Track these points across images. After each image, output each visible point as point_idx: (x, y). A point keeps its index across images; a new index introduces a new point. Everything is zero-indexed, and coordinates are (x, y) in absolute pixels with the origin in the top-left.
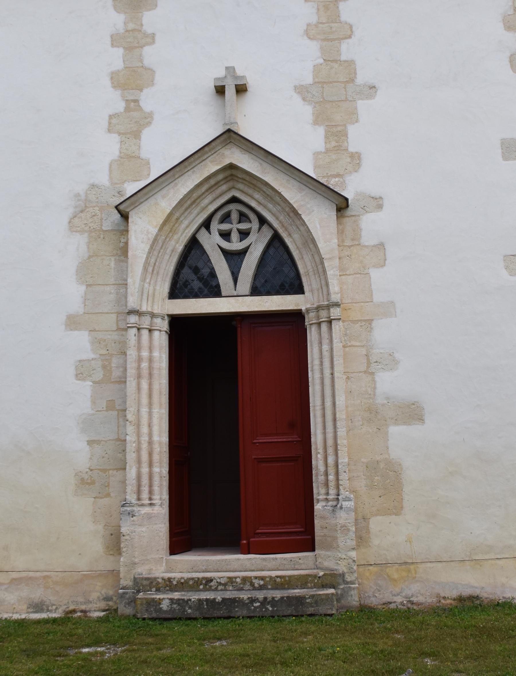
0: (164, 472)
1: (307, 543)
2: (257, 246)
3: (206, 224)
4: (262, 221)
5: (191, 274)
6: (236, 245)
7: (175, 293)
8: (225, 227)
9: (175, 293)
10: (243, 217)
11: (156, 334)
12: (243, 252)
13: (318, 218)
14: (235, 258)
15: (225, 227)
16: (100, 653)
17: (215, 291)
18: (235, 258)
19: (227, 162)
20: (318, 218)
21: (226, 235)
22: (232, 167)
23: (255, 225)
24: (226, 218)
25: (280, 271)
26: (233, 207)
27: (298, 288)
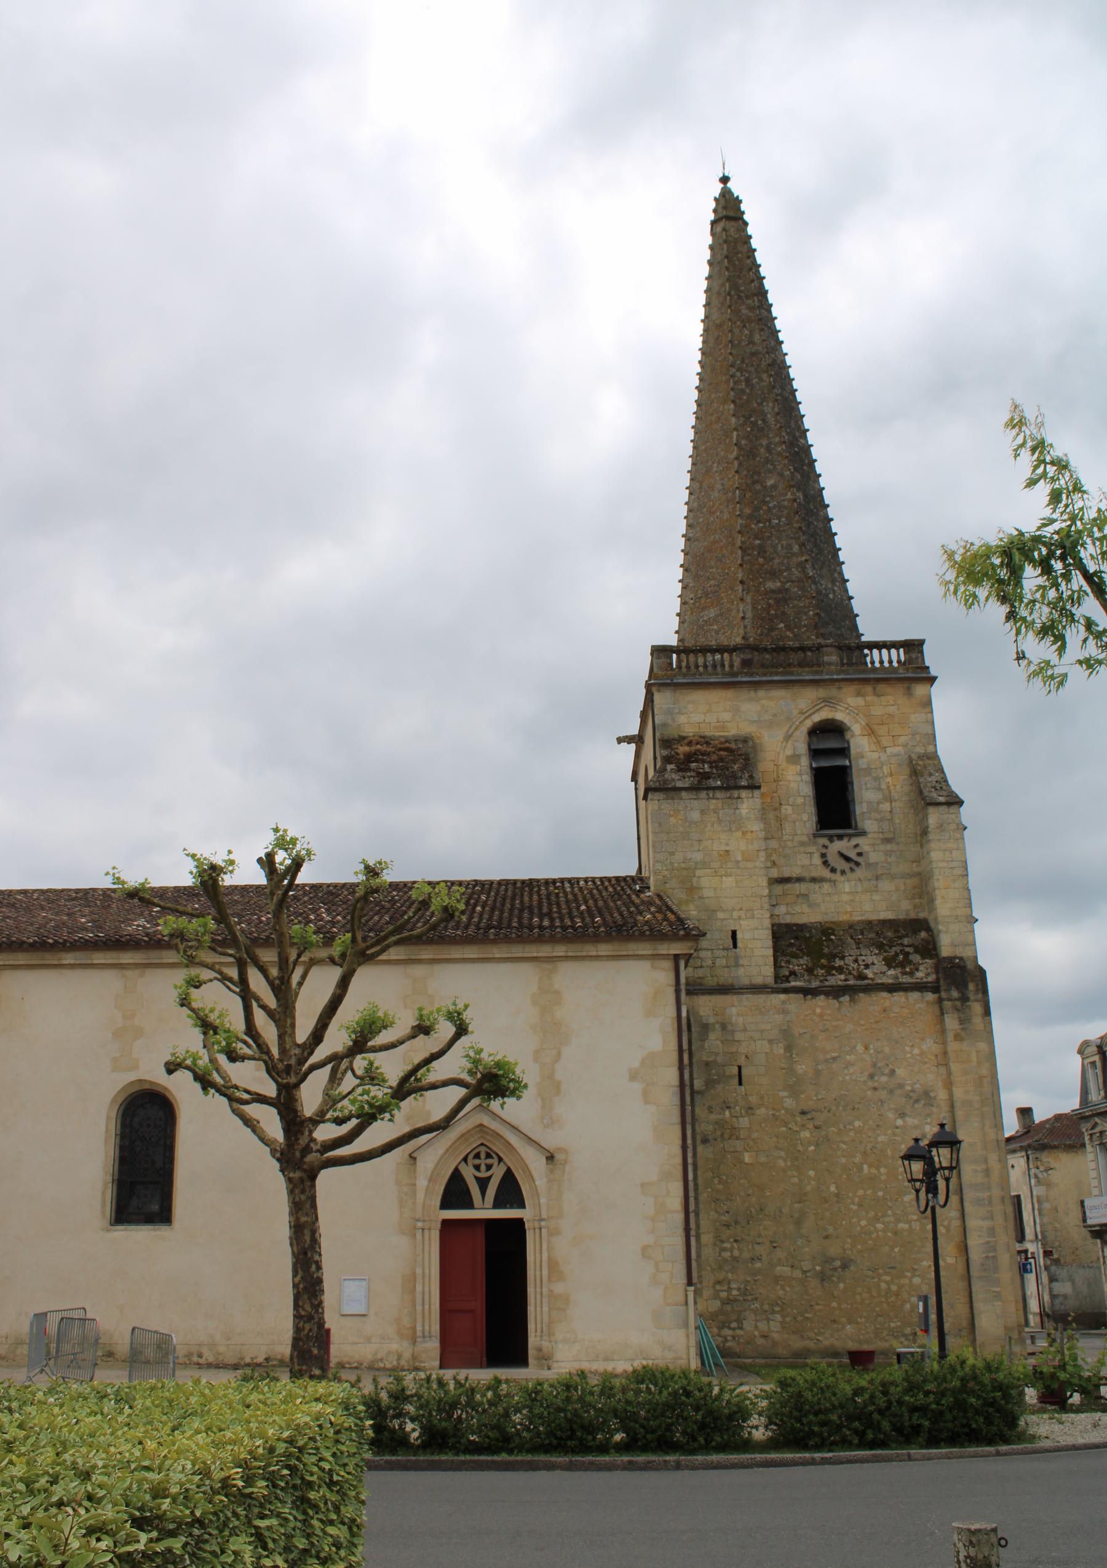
0: (903, 1146)
1: (521, 1359)
2: (498, 1173)
3: (465, 1159)
4: (500, 1160)
5: (455, 1193)
6: (483, 1174)
7: (445, 1204)
8: (477, 1162)
9: (445, 1204)
10: (488, 1156)
11: (433, 1232)
12: (489, 1178)
13: (536, 1162)
14: (483, 1184)
15: (477, 1162)
16: (774, 361)
17: (470, 1205)
18: (483, 1184)
19: (478, 1123)
20: (536, 1162)
21: (477, 1168)
22: (481, 1125)
23: (495, 1161)
24: (477, 1156)
25: (510, 1192)
26: (483, 1150)
27: (522, 1205)
